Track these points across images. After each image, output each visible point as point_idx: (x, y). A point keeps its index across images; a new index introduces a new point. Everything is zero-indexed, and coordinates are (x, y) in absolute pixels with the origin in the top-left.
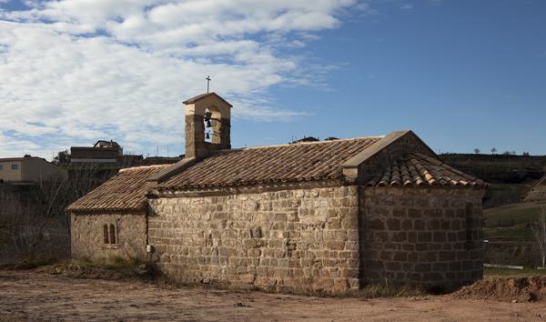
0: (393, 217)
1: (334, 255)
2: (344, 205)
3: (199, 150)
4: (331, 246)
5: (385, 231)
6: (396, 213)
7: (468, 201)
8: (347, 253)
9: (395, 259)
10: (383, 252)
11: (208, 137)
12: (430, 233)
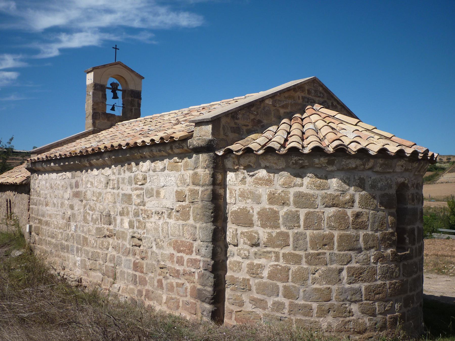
0: (268, 206)
1: (180, 261)
2: (194, 184)
3: (97, 122)
4: (177, 246)
5: (255, 228)
6: (272, 199)
7: (401, 180)
8: (196, 260)
9: (269, 277)
11: (113, 109)
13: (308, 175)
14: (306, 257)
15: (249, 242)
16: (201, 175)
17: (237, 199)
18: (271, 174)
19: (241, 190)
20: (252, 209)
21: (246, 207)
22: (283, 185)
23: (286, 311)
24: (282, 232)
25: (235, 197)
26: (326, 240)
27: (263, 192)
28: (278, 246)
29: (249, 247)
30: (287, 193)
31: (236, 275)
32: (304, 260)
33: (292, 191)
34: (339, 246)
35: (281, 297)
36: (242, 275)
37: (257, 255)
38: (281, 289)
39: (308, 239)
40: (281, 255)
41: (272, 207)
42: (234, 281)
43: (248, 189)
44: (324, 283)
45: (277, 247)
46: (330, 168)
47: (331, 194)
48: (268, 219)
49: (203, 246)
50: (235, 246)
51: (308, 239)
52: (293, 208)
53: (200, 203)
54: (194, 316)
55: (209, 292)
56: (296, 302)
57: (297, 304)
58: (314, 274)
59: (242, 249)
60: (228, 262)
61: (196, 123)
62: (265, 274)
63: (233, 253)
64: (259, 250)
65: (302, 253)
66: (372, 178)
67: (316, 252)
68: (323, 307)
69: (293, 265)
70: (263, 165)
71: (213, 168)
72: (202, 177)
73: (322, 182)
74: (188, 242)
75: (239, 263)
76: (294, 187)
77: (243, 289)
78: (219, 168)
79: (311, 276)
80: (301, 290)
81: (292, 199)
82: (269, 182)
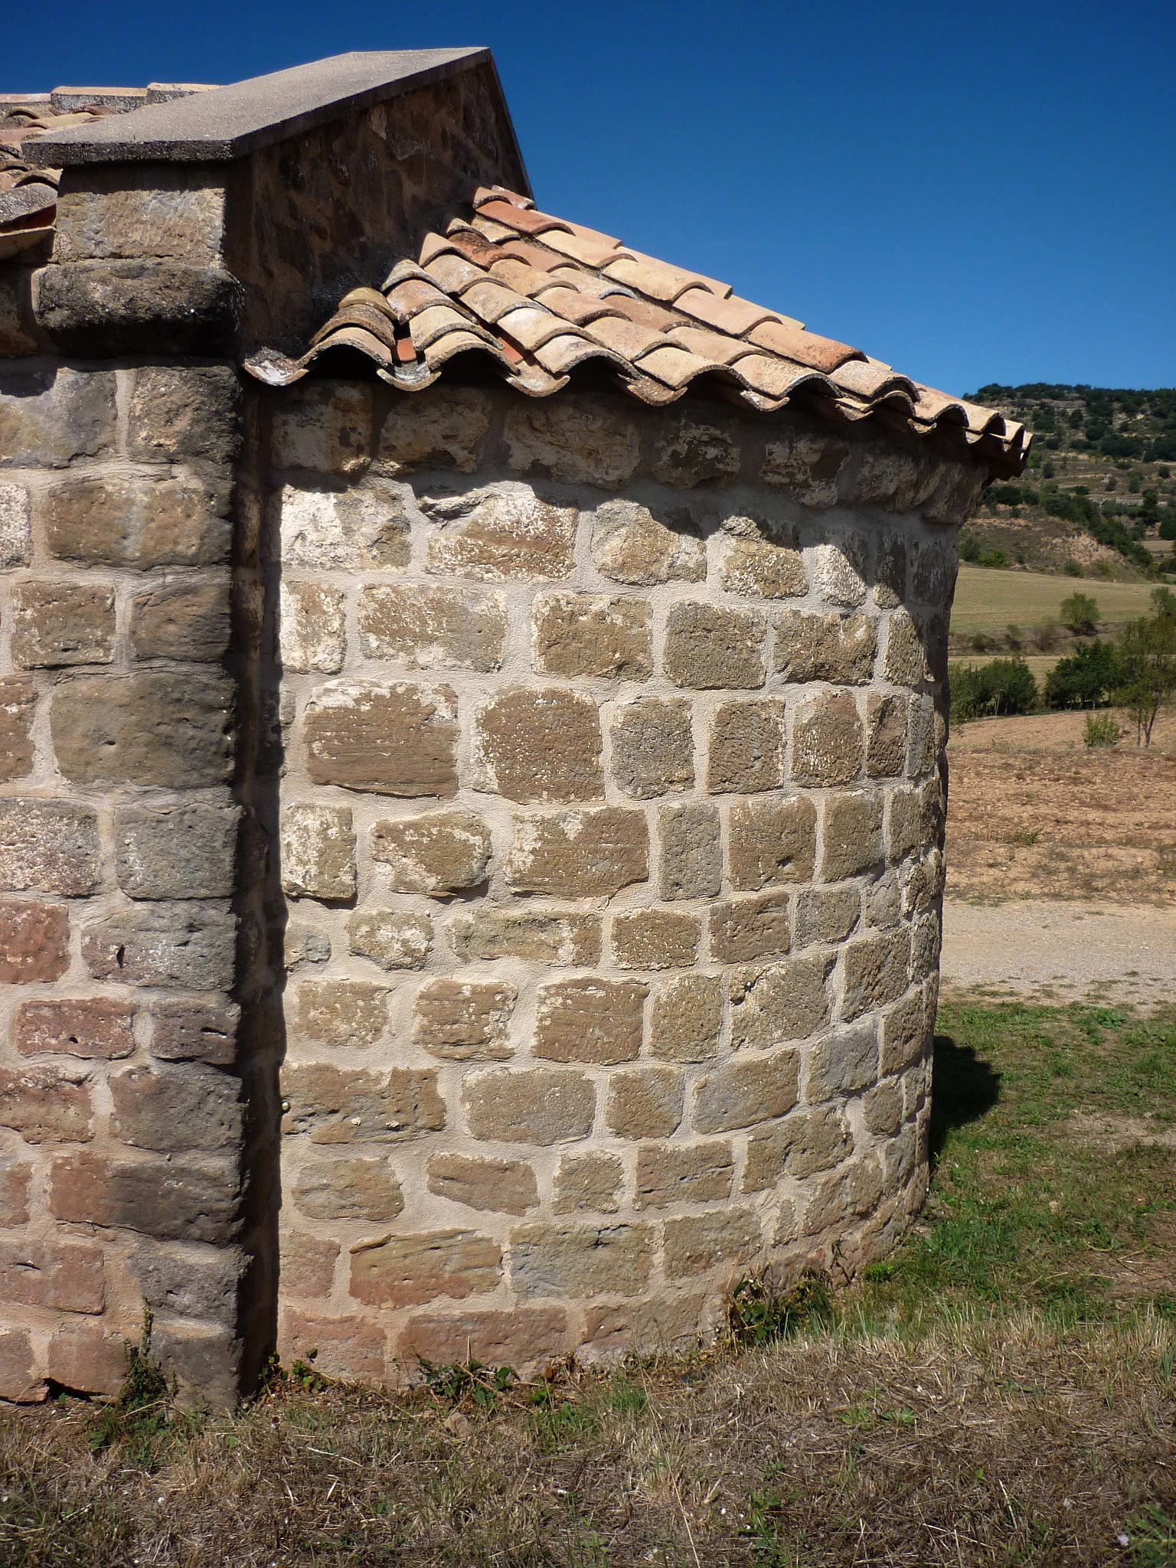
0: (540, 685)
2: (65, 552)
5: (465, 801)
8: (97, 1012)
9: (547, 1050)
10: (448, 993)
12: (810, 811)
13: (731, 521)
14: (716, 928)
15: (432, 881)
16: (130, 502)
17: (354, 644)
18: (560, 512)
19: (380, 593)
20: (451, 697)
21: (413, 690)
22: (613, 573)
23: (625, 1197)
24: (613, 811)
25: (340, 634)
26: (791, 837)
27: (518, 603)
28: (592, 888)
29: (429, 907)
30: (637, 614)
31: (347, 1061)
32: (707, 940)
33: (664, 601)
34: (830, 859)
35: (601, 1136)
36: (382, 1060)
37: (473, 943)
38: (604, 1097)
39: (725, 840)
40: (607, 930)
41: (561, 684)
42: (336, 1095)
43: (423, 590)
44: (777, 1034)
45: (587, 893)
46: (821, 493)
47: (811, 619)
48: (543, 750)
49: (157, 923)
50: (332, 903)
51: (725, 840)
52: (662, 690)
53: (121, 669)
54: (93, 1322)
55: (214, 1180)
56: (670, 1144)
57: (673, 1155)
58: (739, 1001)
59: (383, 917)
60: (291, 995)
61: (69, 171)
62: (522, 1032)
63: (320, 944)
64: (481, 917)
65: (698, 910)
66: (922, 547)
67: (754, 896)
68: (770, 1143)
69: (663, 974)
70: (519, 458)
71: (230, 458)
72: (137, 514)
73: (786, 560)
74: (19, 909)
75: (367, 993)
76: (671, 584)
77: (396, 1129)
78: (256, 456)
79: (730, 1012)
80: (691, 1086)
81: (659, 643)
82: (546, 553)
